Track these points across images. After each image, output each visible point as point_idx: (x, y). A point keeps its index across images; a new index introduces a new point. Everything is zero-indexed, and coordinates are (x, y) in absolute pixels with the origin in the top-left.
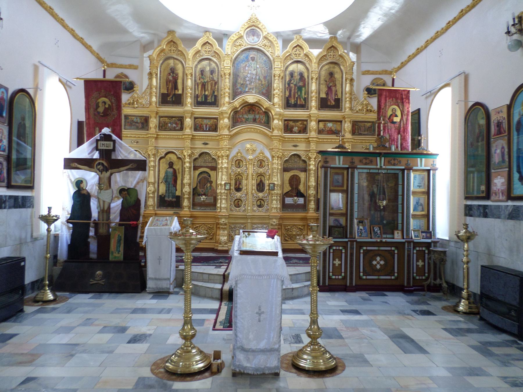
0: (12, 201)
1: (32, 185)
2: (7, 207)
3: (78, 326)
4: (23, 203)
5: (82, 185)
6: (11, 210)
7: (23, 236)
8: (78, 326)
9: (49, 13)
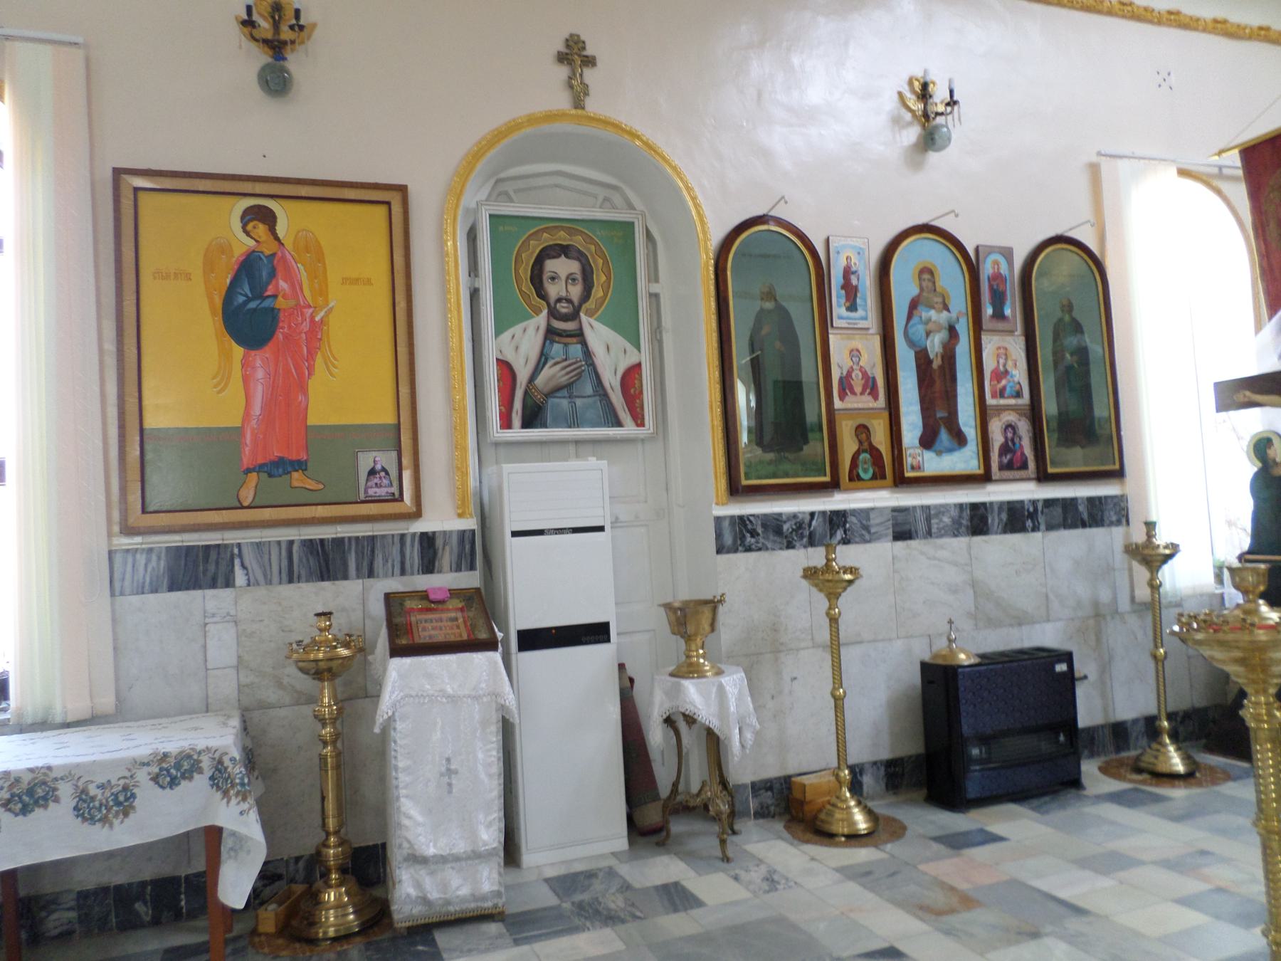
0: (1058, 511)
1: (1117, 467)
2: (1043, 527)
3: (1154, 863)
4: (1091, 515)
5: (1271, 453)
6: (1054, 535)
7: (1105, 595)
8: (1154, 863)
9: (1124, 17)
